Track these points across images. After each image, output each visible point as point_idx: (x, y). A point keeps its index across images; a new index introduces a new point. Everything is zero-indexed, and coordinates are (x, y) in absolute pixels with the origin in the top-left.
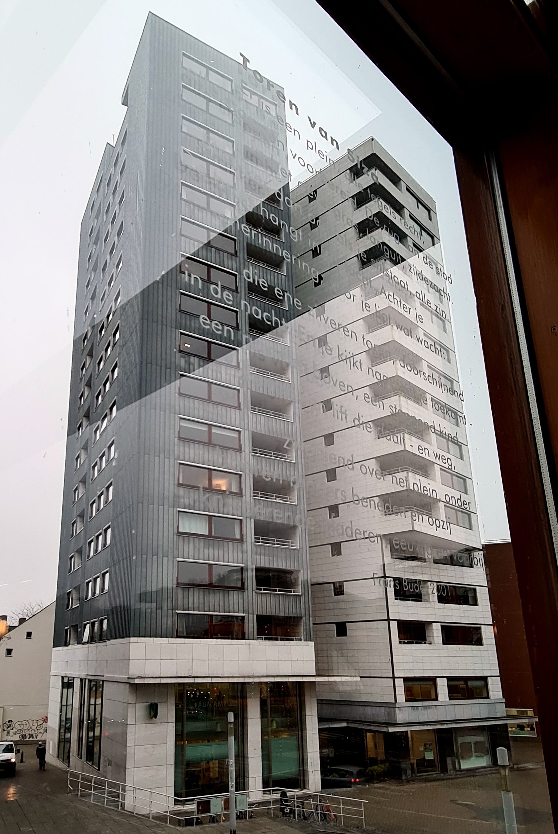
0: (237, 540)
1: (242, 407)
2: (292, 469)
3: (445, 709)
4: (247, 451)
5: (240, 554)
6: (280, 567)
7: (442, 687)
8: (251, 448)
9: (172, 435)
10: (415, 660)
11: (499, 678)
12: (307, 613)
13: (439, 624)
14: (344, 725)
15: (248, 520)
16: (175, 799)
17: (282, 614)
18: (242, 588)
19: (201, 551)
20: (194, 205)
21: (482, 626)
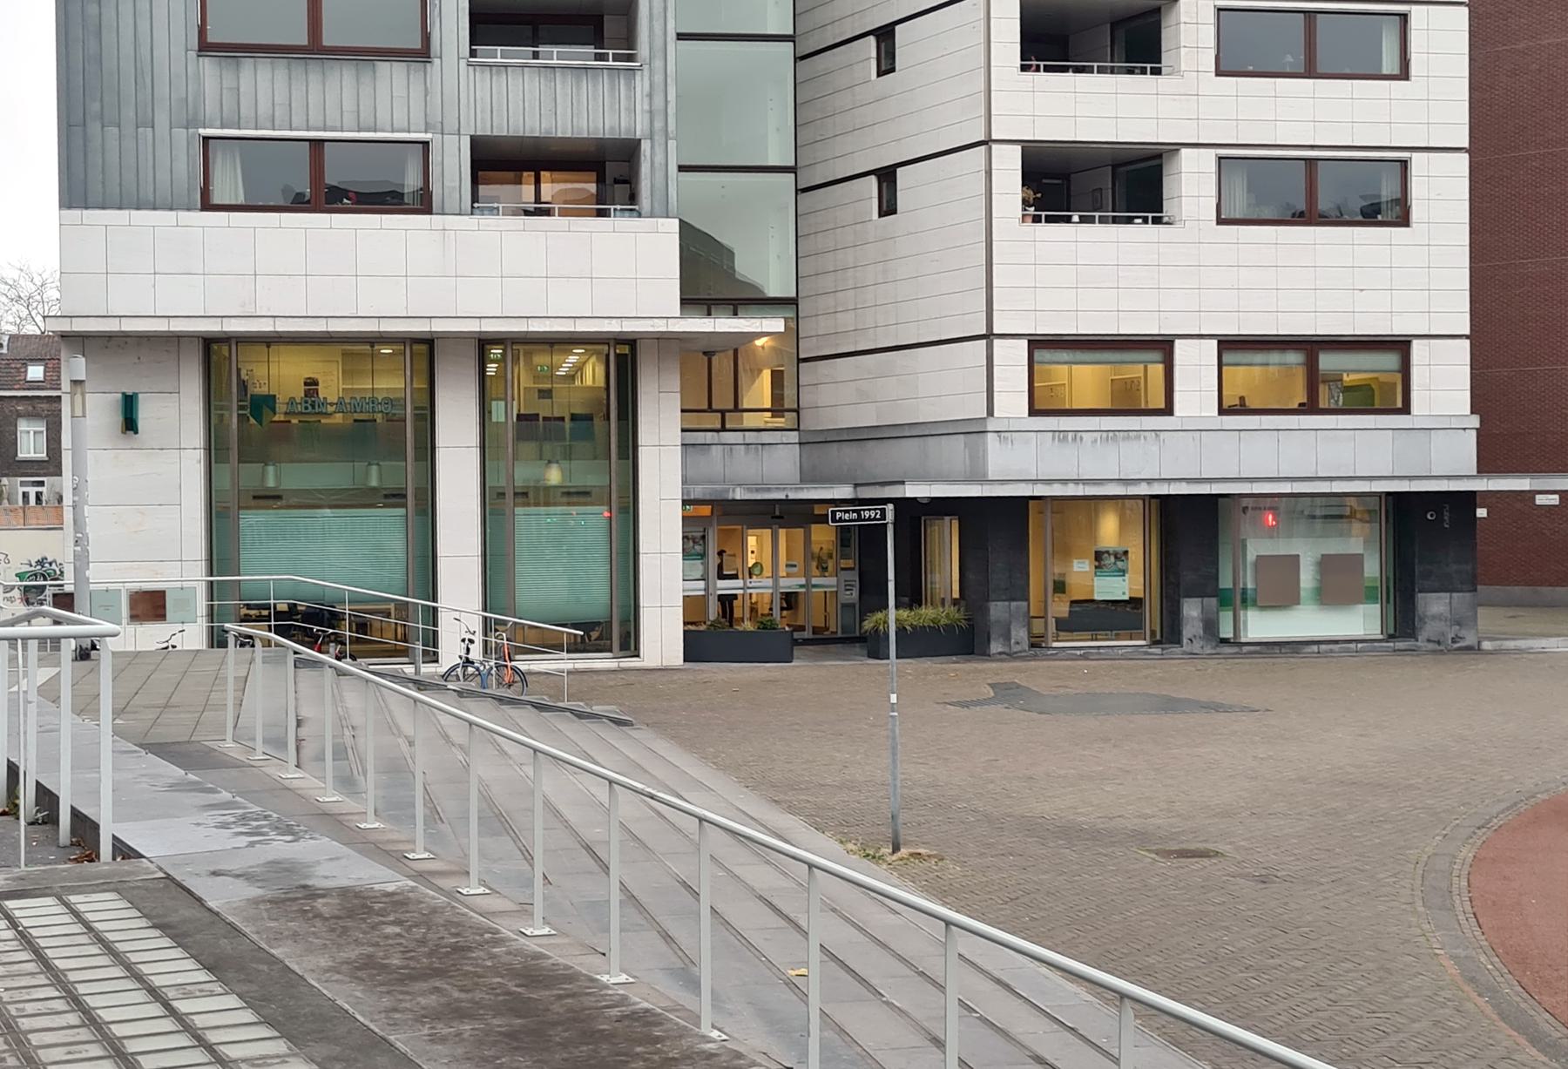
3: (1197, 444)
7: (1196, 370)
10: (1088, 274)
12: (658, 125)
13: (1213, 152)
17: (560, 135)
18: (422, 54)
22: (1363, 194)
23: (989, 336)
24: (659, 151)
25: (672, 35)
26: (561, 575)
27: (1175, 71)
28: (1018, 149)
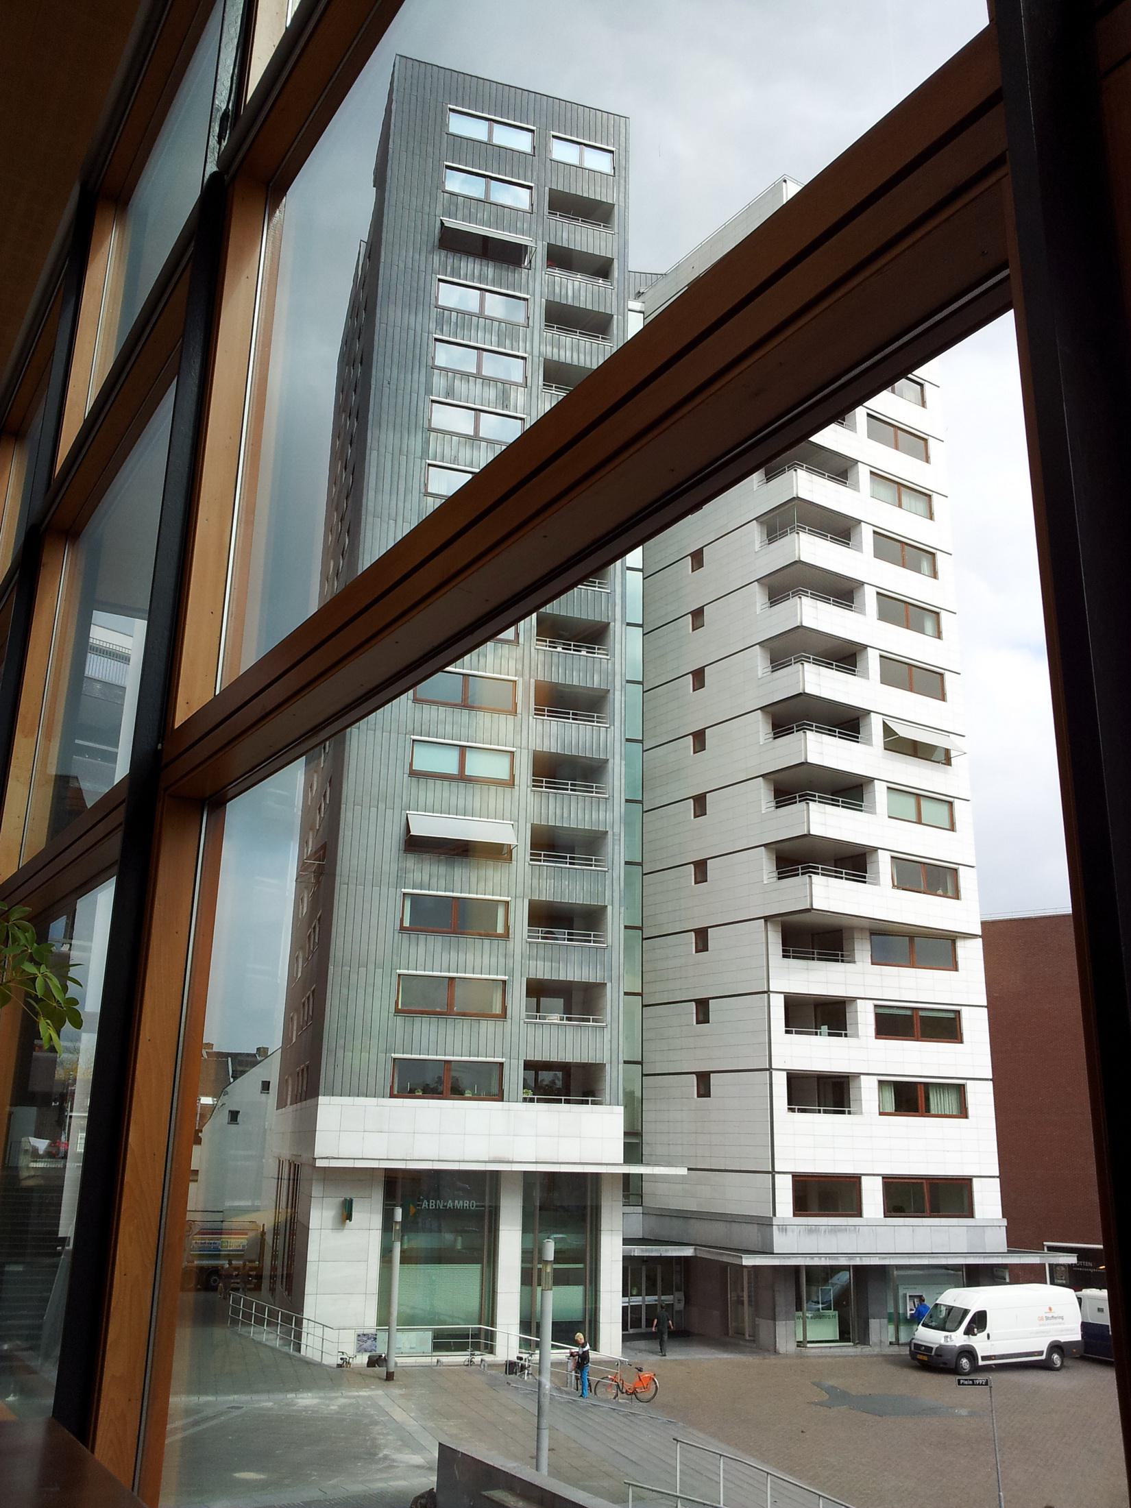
0: (499, 936)
1: (519, 711)
2: (602, 807)
4: (523, 787)
5: (502, 960)
6: (570, 978)
7: (873, 1197)
8: (530, 777)
9: (399, 772)
10: (813, 1143)
11: (998, 1180)
14: (688, 1252)
15: (519, 901)
16: (966, 1312)
19: (437, 956)
20: (455, 372)
21: (969, 1082)
22: (943, 1026)
23: (768, 992)
24: (615, 1070)
25: (621, 1061)
26: (558, 1301)
27: (857, 1036)
28: (790, 1176)
